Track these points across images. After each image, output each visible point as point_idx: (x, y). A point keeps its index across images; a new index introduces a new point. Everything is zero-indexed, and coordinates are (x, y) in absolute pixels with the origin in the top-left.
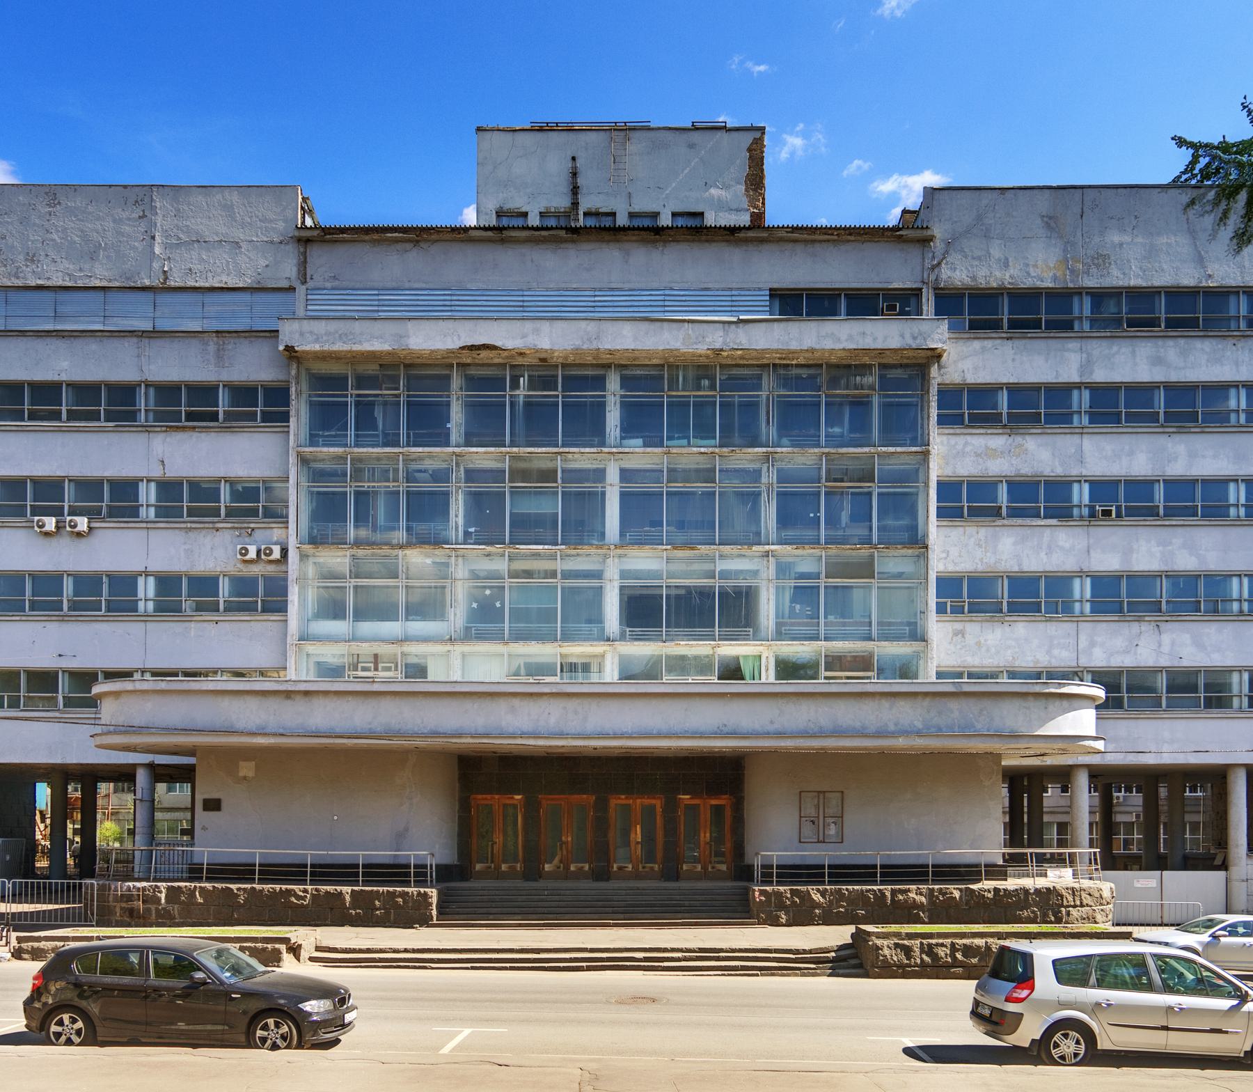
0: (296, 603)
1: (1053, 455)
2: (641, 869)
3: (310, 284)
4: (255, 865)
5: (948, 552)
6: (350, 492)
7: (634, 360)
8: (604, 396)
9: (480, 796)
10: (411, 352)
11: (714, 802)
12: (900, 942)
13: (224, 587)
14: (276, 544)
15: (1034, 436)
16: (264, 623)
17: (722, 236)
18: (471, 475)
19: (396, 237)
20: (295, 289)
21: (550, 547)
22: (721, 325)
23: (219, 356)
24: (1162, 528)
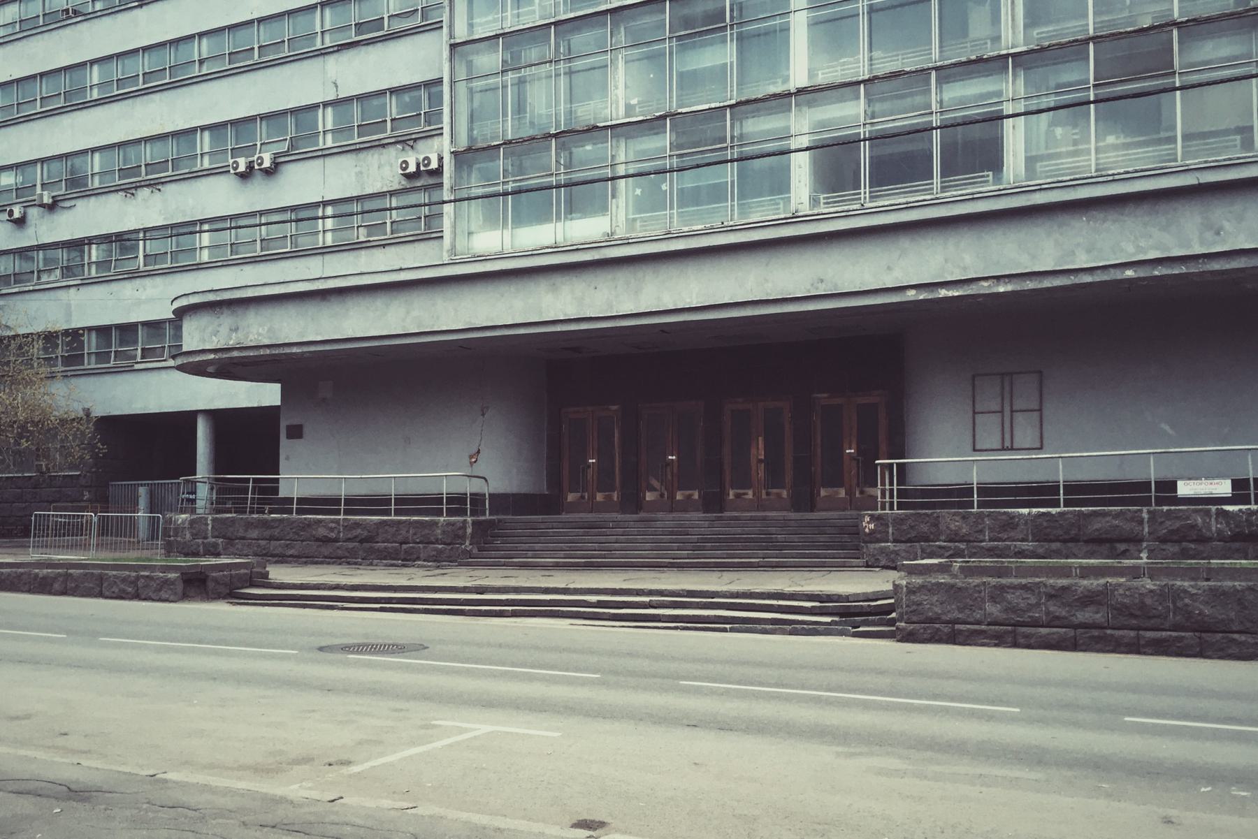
2: (764, 496)
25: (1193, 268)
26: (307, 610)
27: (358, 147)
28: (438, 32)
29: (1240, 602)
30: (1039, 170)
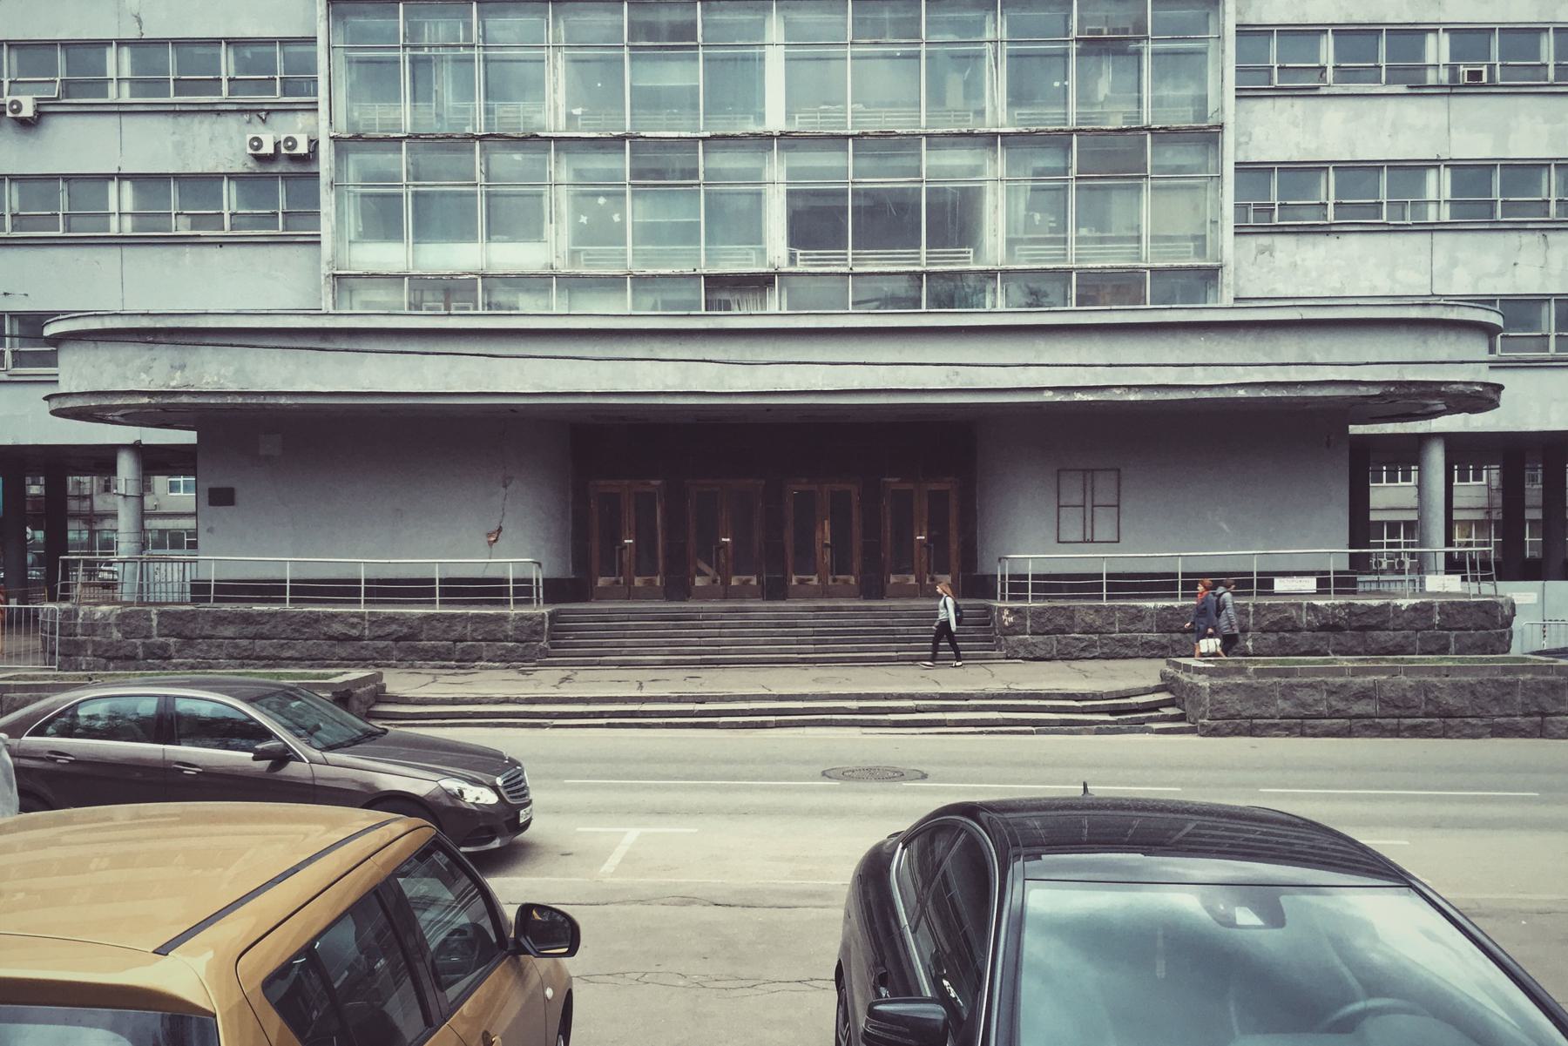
2: (830, 583)
4: (285, 581)
5: (1251, 134)
6: (404, 57)
9: (602, 482)
11: (934, 487)
14: (301, 132)
24: (890, 316)
25: (1293, 393)
27: (178, 108)
29: (1473, 693)
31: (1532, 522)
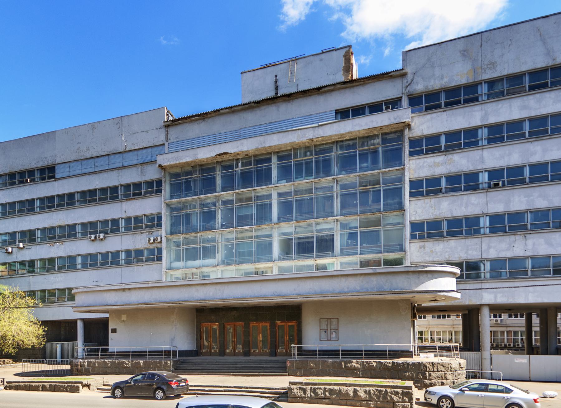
0: (165, 257)
1: (468, 161)
2: (262, 352)
3: (170, 141)
4: (114, 352)
5: (416, 211)
7: (280, 149)
8: (271, 165)
10: (200, 160)
11: (290, 324)
12: (302, 387)
13: (145, 253)
15: (458, 154)
16: (157, 265)
17: (315, 92)
18: (225, 203)
19: (196, 119)
20: (164, 144)
21: (250, 227)
22: (312, 128)
23: (142, 172)
26: (215, 385)
28: (161, 197)
30: (344, 252)
31: (535, 332)
